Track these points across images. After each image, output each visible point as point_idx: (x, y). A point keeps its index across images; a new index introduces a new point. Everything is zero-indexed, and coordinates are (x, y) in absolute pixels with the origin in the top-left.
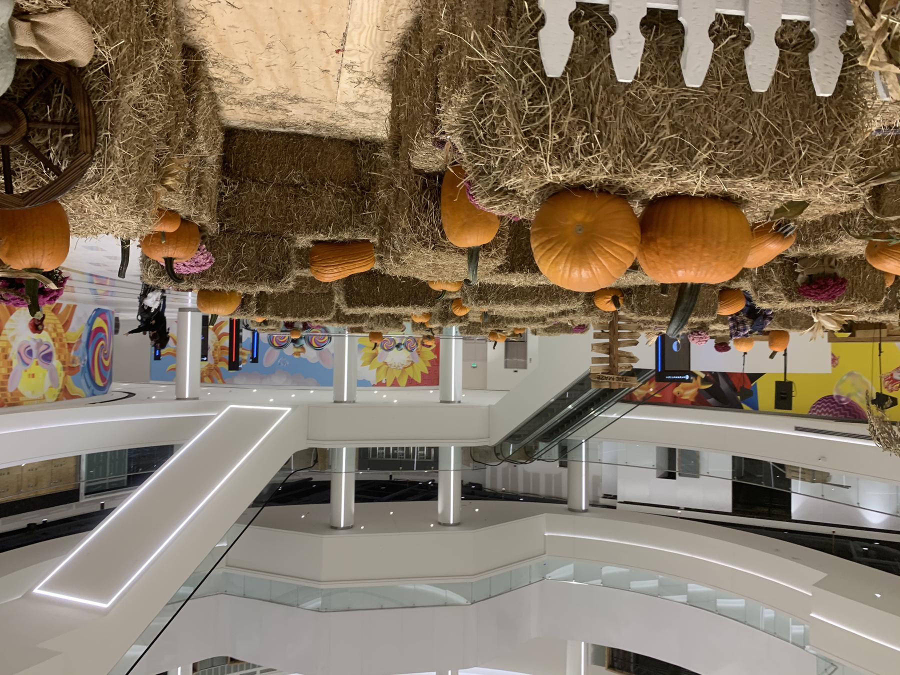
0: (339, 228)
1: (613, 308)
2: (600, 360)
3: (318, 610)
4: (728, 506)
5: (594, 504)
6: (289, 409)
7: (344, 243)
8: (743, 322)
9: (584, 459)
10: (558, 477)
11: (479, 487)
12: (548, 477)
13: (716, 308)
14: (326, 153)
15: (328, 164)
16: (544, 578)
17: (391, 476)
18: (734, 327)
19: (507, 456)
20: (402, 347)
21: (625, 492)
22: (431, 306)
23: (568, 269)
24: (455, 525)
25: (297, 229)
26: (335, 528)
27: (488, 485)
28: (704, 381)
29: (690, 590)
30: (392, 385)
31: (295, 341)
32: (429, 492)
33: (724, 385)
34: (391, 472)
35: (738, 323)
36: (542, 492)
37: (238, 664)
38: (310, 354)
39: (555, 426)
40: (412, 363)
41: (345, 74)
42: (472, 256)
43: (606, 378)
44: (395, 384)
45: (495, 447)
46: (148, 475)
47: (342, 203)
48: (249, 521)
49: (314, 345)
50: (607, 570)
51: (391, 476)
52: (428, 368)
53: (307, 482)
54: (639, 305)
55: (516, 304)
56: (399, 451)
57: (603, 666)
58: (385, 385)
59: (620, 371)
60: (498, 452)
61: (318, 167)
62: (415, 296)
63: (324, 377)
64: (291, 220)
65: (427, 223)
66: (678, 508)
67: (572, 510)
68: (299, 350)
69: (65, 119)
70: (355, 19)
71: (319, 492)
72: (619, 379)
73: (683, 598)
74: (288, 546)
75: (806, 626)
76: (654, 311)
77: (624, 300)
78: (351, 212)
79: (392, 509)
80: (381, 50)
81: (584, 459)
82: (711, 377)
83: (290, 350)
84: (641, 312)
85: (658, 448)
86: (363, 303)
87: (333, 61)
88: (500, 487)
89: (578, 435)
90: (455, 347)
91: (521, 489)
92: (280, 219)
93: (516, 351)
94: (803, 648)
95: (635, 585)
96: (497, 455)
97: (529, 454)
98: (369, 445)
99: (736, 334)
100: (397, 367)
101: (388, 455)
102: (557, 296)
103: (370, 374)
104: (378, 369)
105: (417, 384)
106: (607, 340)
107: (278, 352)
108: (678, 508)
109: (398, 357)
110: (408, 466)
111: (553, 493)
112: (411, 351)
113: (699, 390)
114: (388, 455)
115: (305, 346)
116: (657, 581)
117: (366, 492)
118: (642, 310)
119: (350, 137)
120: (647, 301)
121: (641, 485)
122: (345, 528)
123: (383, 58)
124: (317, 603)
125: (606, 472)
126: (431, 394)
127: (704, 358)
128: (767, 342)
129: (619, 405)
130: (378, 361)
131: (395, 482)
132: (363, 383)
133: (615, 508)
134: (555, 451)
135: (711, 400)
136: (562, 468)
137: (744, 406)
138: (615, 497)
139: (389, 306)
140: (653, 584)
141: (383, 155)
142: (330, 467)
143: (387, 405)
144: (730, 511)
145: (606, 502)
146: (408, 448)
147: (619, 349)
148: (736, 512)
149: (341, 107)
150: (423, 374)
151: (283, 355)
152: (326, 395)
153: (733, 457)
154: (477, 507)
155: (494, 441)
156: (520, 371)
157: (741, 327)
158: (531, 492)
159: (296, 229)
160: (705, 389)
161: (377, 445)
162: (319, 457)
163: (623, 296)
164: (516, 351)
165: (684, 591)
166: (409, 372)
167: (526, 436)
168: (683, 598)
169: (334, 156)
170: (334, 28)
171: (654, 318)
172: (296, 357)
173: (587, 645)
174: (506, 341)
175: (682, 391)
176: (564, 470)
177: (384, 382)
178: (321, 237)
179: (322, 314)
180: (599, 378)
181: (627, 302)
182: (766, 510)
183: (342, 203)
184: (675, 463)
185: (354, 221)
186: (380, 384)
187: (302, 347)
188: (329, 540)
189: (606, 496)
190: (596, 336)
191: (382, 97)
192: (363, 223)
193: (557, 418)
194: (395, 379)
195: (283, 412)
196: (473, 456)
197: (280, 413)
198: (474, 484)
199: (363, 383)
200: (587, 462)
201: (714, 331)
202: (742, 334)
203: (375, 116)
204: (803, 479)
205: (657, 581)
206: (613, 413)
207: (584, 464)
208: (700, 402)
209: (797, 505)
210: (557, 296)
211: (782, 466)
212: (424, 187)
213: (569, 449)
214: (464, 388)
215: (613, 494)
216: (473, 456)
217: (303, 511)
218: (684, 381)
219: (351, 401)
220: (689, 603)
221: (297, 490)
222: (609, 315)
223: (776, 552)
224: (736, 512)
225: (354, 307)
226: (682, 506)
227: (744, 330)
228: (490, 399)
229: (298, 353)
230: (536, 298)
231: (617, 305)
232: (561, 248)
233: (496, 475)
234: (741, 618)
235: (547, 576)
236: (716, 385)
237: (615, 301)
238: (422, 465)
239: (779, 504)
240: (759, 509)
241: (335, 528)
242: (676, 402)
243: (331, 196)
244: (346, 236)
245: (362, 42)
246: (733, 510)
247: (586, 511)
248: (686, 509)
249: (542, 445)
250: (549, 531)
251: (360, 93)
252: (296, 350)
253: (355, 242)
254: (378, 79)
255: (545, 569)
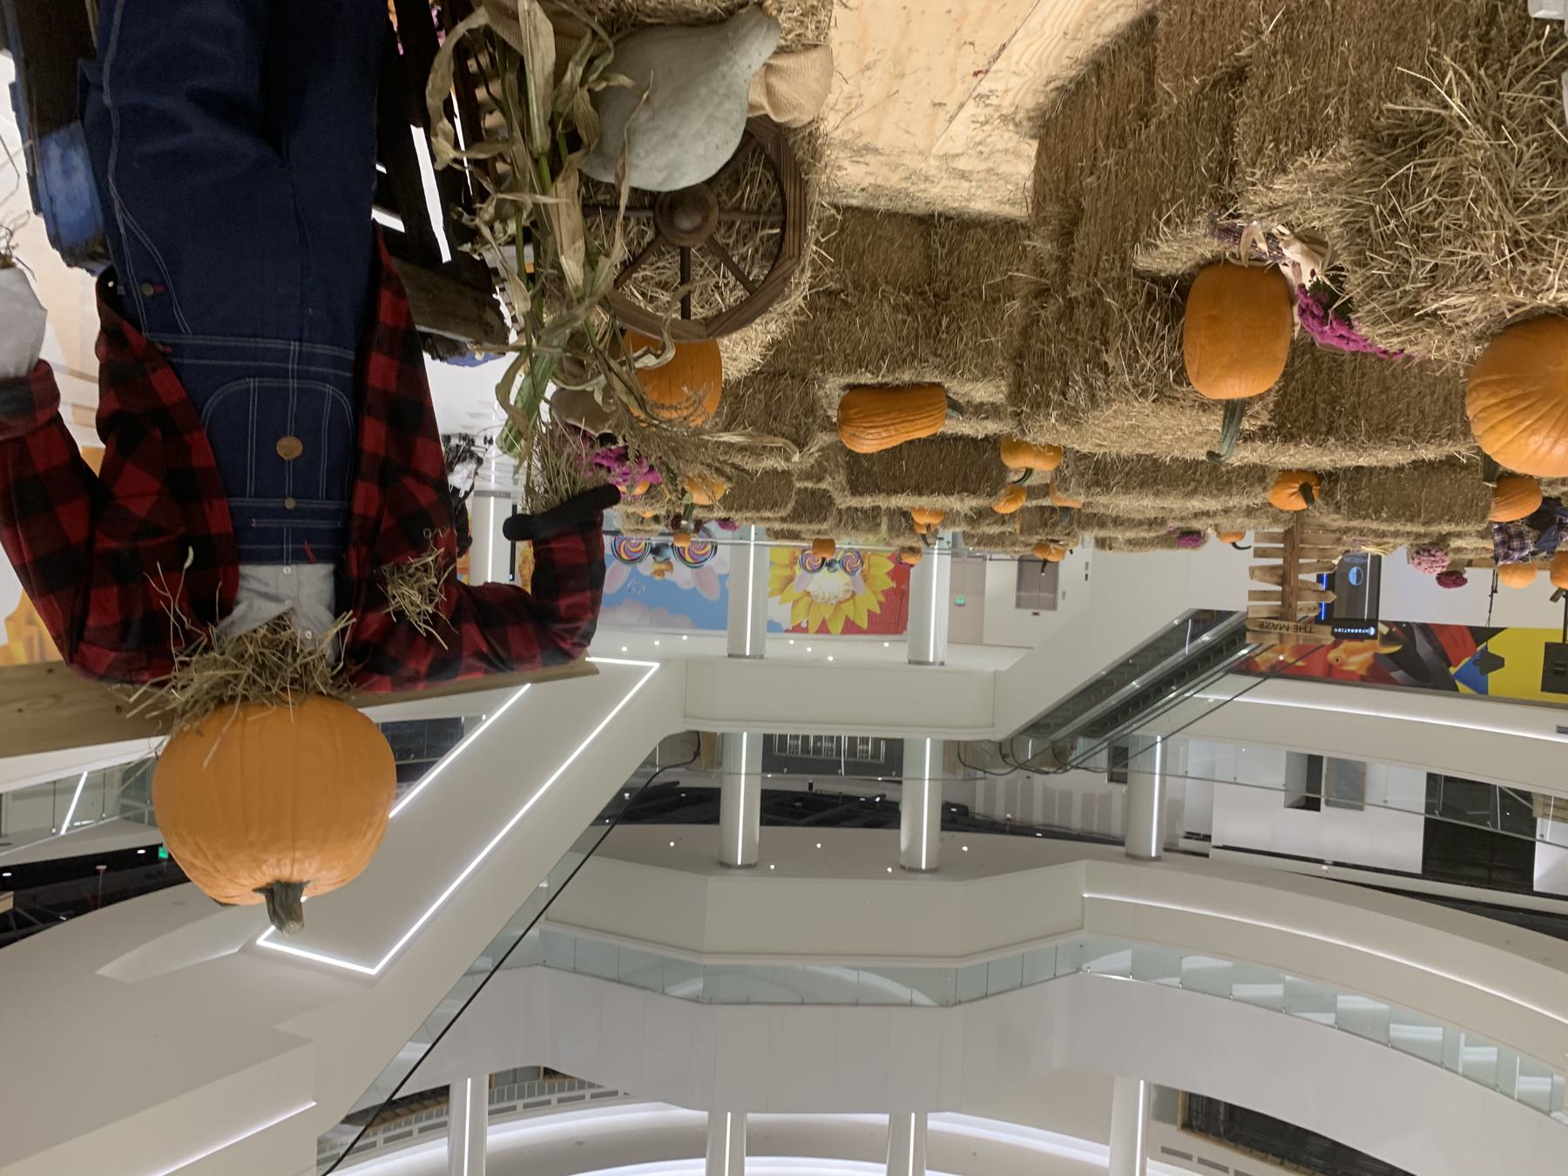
0: (897, 364)
1: (1299, 504)
2: (1265, 595)
3: (695, 1000)
4: (1415, 862)
5: (1169, 848)
6: (656, 666)
7: (898, 389)
8: (1520, 536)
9: (1157, 770)
10: (1107, 799)
11: (964, 810)
12: (1088, 799)
13: (1487, 508)
14: (880, 237)
15: (882, 257)
16: (1078, 970)
17: (811, 786)
18: (1503, 543)
19: (1022, 760)
20: (837, 566)
21: (1226, 829)
22: (989, 495)
23: (1551, 440)
24: (929, 871)
25: (830, 365)
26: (726, 865)
27: (979, 809)
28: (1388, 639)
29: (1340, 1005)
30: (818, 632)
31: (656, 551)
32: (885, 815)
33: (1423, 648)
34: (810, 778)
35: (1511, 537)
36: (1076, 824)
37: (567, 1082)
38: (681, 575)
39: (1109, 714)
40: (854, 594)
41: (971, 109)
42: (1233, 415)
43: (1275, 627)
44: (823, 629)
45: (1000, 745)
46: (429, 766)
47: (904, 322)
48: (591, 848)
49: (688, 559)
50: (1193, 963)
51: (811, 786)
52: (880, 603)
53: (671, 789)
54: (1351, 500)
55: (1157, 494)
56: (825, 744)
57: (1174, 1122)
58: (806, 630)
59: (1300, 615)
60: (1005, 751)
61: (867, 259)
62: (965, 478)
63: (711, 613)
64: (821, 350)
65: (1152, 358)
66: (1321, 862)
67: (1133, 857)
68: (663, 567)
69: (760, 206)
70: (1034, 22)
71: (703, 806)
72: (1297, 629)
73: (1329, 1018)
74: (647, 890)
75: (1558, 1079)
76: (1377, 512)
77: (1321, 492)
78: (917, 336)
79: (819, 839)
80: (1053, 70)
81: (1157, 770)
82: (1403, 632)
83: (648, 565)
84: (1353, 515)
85: (1289, 754)
86: (876, 489)
87: (960, 88)
88: (1001, 812)
89: (1152, 730)
90: (936, 573)
91: (1037, 818)
92: (804, 349)
93: (1037, 581)
94: (1548, 1113)
95: (1240, 990)
96: (1004, 757)
97: (1059, 759)
98: (776, 731)
99: (1506, 557)
100: (827, 602)
101: (805, 750)
102: (1229, 481)
103: (781, 611)
104: (795, 603)
105: (860, 631)
106: (1280, 561)
107: (627, 569)
108: (1321, 862)
109: (831, 583)
110: (830, 767)
111: (1096, 827)
112: (852, 573)
113: (1376, 656)
114: (805, 750)
115: (673, 560)
116: (1281, 987)
117: (779, 809)
118: (1356, 510)
119: (921, 209)
120: (1365, 494)
121: (1257, 817)
122: (745, 866)
123: (1049, 82)
124: (695, 986)
125: (1192, 794)
126: (888, 649)
127: (1410, 594)
128: (1547, 574)
129: (1231, 678)
130: (794, 590)
131: (833, 794)
132: (773, 627)
133: (1207, 856)
134: (1102, 759)
135: (1397, 674)
136: (1114, 785)
137: (1459, 684)
138: (1208, 838)
139: (921, 494)
140: (1276, 990)
141: (1038, 244)
142: (720, 764)
143: (816, 665)
144: (1419, 870)
145: (1192, 846)
146: (806, 738)
147: (1301, 577)
148: (1428, 872)
149: (933, 162)
150: (871, 614)
151: (635, 574)
152: (714, 644)
153: (1432, 778)
154: (966, 844)
155: (1000, 734)
156: (1043, 613)
157: (1516, 544)
158: (1056, 823)
159: (828, 366)
160: (1389, 655)
161: (789, 731)
162: (700, 746)
163: (1319, 484)
164: (1037, 581)
165: (1331, 1007)
166: (848, 609)
167: (1059, 726)
168: (1329, 1018)
169: (892, 241)
170: (988, 39)
171: (1374, 525)
172: (658, 578)
173: (1148, 1087)
174: (1021, 560)
175: (1343, 656)
176: (1119, 790)
177: (804, 625)
178: (867, 378)
179: (774, 506)
180: (1262, 625)
181: (1328, 495)
182: (1481, 873)
183: (904, 322)
184: (1318, 783)
185: (923, 351)
186: (798, 629)
187: (667, 561)
188: (717, 885)
189: (1190, 836)
190: (1259, 553)
191: (1010, 145)
192: (936, 355)
193: (1113, 700)
194: (824, 621)
195: (644, 670)
196: (962, 757)
197: (641, 671)
198: (954, 806)
199: (773, 627)
200: (1163, 775)
201: (1459, 550)
202: (1516, 555)
203: (983, 175)
204: (1555, 818)
205: (1281, 987)
206: (1211, 693)
207: (1157, 778)
208: (1376, 676)
209: (1544, 863)
210: (1229, 481)
211: (1527, 796)
212: (1150, 297)
213: (1131, 752)
214: (952, 641)
215: (1203, 832)
216: (962, 757)
217: (672, 836)
218: (1367, 636)
219: (758, 656)
220: (1339, 1027)
221: (665, 802)
222: (1288, 516)
223: (1508, 945)
224: (1428, 872)
225: (861, 494)
226: (1330, 858)
227: (1522, 549)
228: (1002, 662)
229: (661, 573)
230: (1193, 484)
231: (1309, 498)
232: (1547, 408)
233: (995, 793)
234: (1441, 1058)
235: (1084, 966)
236: (1409, 646)
237: (1306, 492)
238: (859, 767)
239: (1511, 860)
240: (1468, 871)
241: (726, 865)
242: (1333, 675)
243: (887, 309)
244: (907, 376)
245: (1025, 59)
246: (1424, 870)
247: (1157, 859)
248: (1336, 864)
249: (1082, 744)
250: (1089, 890)
251: (977, 139)
252: (657, 567)
253: (917, 386)
254: (1020, 116)
255: (1079, 958)
